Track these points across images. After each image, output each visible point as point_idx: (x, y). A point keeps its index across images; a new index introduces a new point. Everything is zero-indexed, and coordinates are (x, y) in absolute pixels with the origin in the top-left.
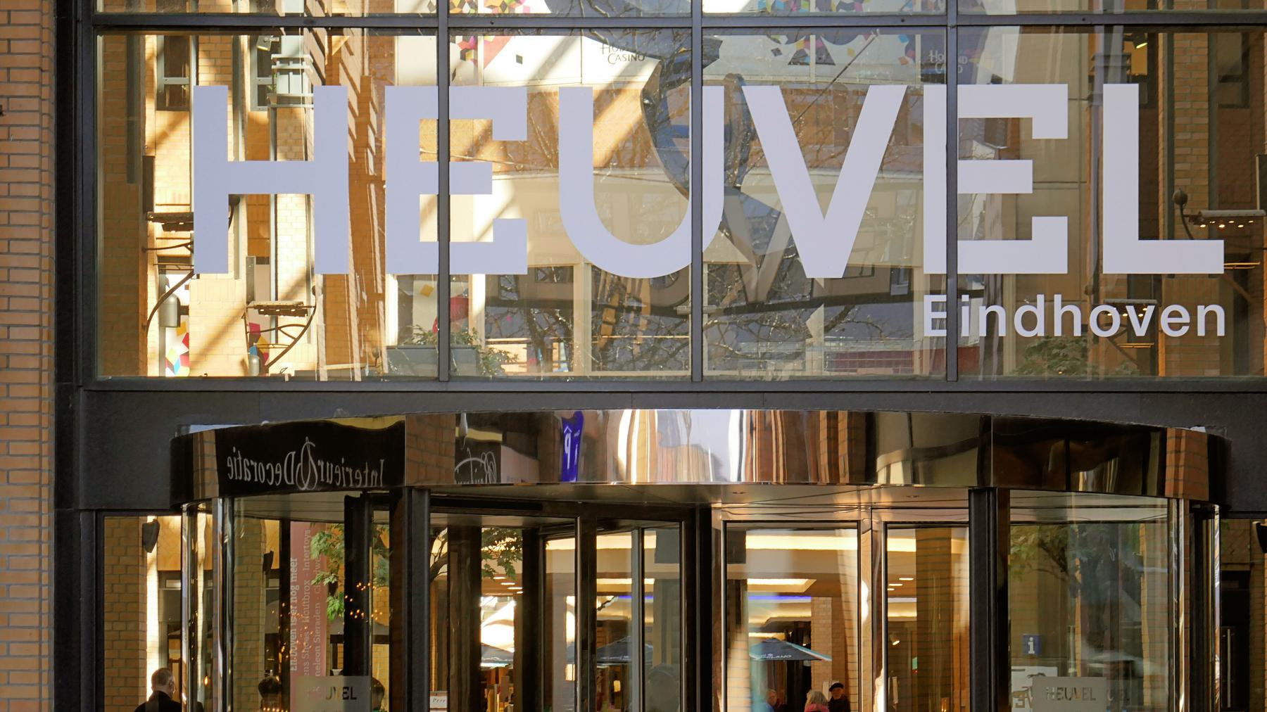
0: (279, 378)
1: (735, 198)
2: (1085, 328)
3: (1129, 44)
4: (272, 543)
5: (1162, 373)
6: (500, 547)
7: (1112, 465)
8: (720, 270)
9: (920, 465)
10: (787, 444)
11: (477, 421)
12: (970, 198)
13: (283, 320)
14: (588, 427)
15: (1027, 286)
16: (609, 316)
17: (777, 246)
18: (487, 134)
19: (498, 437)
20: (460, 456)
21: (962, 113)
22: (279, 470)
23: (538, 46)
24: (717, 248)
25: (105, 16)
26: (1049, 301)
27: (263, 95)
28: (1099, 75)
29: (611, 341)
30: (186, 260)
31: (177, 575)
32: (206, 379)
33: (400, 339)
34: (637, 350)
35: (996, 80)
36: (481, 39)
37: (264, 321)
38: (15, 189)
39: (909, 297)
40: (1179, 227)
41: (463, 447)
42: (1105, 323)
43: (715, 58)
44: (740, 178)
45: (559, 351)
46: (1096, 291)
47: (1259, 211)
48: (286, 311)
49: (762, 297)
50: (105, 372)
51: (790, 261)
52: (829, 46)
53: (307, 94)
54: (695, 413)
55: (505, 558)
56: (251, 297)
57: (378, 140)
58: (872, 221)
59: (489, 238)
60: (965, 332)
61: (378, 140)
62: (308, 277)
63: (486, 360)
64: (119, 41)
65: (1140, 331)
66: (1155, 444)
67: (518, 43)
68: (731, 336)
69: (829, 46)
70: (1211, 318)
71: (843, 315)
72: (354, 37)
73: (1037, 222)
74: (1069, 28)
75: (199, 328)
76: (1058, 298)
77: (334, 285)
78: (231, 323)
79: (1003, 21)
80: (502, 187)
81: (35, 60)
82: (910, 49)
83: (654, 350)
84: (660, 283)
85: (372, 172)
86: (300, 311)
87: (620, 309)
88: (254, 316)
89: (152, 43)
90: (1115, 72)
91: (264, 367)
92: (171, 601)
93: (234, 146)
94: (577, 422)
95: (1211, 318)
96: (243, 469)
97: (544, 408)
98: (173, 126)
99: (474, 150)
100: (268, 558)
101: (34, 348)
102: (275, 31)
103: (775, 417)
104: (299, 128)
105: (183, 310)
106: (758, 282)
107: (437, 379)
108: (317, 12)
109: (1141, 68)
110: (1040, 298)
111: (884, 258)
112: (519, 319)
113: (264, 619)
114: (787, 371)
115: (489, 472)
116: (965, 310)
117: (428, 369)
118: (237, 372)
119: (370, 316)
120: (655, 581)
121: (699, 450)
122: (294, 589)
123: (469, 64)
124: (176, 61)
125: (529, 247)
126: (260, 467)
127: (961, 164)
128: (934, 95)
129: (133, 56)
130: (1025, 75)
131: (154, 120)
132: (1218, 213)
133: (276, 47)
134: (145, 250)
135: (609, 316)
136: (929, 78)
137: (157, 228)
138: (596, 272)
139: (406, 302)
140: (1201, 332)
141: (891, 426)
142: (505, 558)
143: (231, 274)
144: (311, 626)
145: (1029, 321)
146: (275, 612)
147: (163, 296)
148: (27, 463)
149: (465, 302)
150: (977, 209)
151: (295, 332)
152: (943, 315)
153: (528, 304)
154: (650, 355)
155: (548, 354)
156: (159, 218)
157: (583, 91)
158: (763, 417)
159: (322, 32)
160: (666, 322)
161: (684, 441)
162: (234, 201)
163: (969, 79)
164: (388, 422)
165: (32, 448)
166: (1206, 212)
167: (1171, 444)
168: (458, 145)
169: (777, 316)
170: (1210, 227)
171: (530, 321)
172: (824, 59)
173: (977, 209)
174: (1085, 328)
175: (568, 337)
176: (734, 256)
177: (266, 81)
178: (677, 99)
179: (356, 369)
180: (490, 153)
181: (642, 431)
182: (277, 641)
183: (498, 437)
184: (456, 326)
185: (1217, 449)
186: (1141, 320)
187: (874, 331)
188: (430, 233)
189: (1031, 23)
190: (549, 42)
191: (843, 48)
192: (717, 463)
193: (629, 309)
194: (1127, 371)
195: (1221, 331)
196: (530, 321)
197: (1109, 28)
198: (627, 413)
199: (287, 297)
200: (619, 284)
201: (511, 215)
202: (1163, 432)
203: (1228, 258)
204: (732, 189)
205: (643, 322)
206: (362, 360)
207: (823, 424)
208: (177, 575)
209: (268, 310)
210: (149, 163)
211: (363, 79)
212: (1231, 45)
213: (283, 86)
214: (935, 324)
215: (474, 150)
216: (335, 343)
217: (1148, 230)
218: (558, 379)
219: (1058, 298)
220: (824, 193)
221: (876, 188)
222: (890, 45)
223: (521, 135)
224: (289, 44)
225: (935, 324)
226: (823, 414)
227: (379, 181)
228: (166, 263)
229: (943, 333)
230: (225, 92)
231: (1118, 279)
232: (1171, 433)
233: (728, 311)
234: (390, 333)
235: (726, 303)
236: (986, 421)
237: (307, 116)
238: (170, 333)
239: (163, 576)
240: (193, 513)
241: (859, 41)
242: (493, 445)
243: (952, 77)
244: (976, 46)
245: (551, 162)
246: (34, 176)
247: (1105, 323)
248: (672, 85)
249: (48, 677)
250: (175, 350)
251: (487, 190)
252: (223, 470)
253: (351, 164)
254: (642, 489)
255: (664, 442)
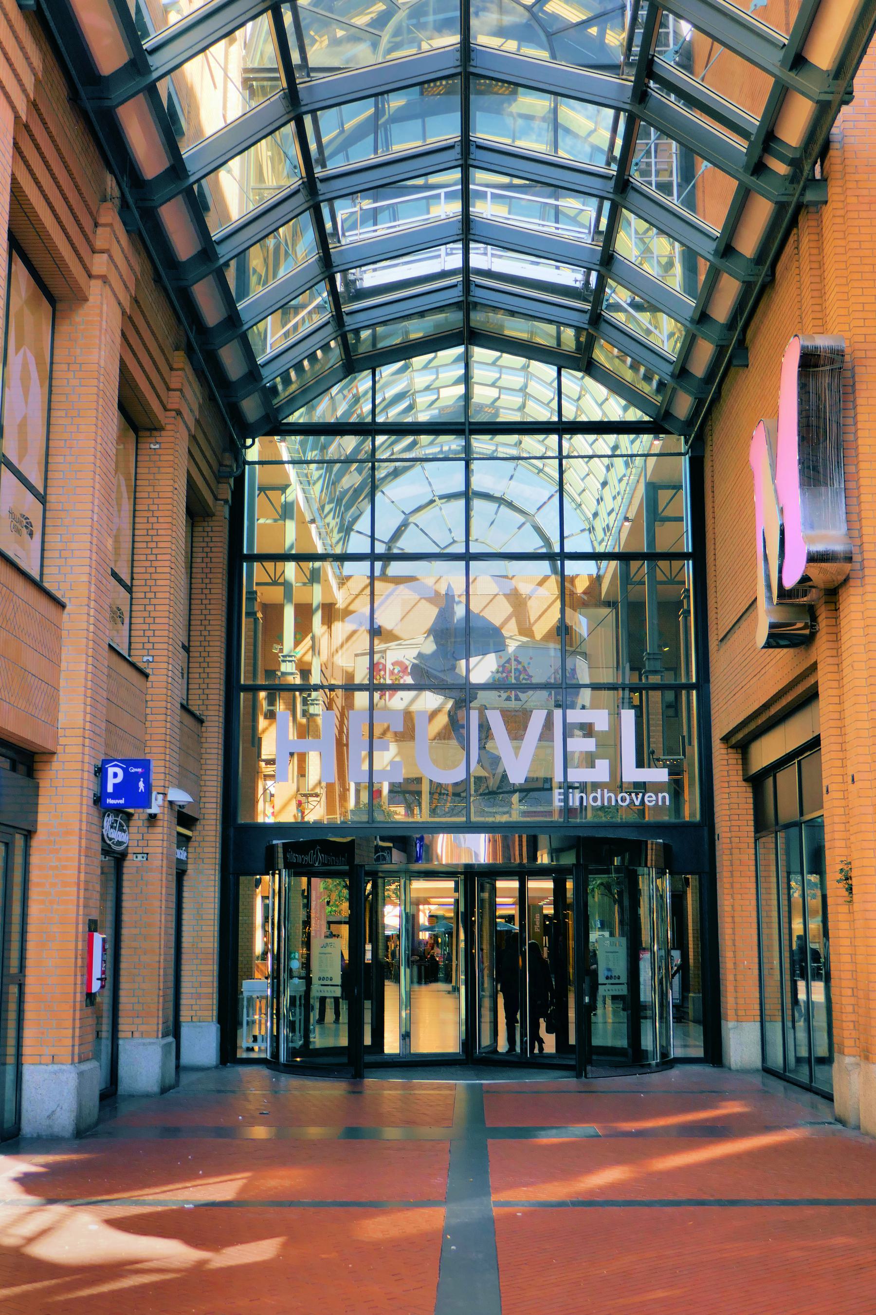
0: (308, 823)
1: (484, 751)
2: (617, 801)
3: (632, 694)
4: (304, 886)
5: (647, 819)
6: (393, 887)
7: (627, 856)
8: (479, 779)
9: (554, 855)
10: (503, 847)
11: (383, 839)
12: (573, 753)
13: (310, 799)
14: (426, 841)
15: (595, 786)
16: (436, 796)
17: (500, 770)
18: (388, 728)
19: (391, 845)
20: (376, 852)
21: (568, 721)
22: (307, 858)
23: (410, 694)
24: (476, 769)
25: (244, 685)
26: (602, 791)
27: (305, 713)
28: (621, 705)
29: (436, 806)
30: (273, 776)
31: (268, 898)
32: (279, 823)
33: (355, 806)
34: (447, 810)
35: (583, 707)
36: (387, 693)
37: (303, 799)
38: (208, 751)
39: (551, 789)
40: (652, 763)
41: (378, 849)
42: (623, 799)
43: (476, 698)
44: (485, 743)
45: (416, 810)
46: (621, 787)
47: (682, 757)
48: (311, 795)
49: (495, 789)
50: (242, 820)
51: (505, 777)
52: (520, 694)
53: (321, 713)
54: (467, 835)
55: (395, 891)
56: (298, 790)
57: (347, 730)
58: (536, 759)
59: (389, 768)
60: (571, 804)
61: (347, 730)
62: (320, 783)
63: (389, 814)
64: (250, 695)
65: (637, 803)
66: (643, 847)
67: (400, 694)
68: (483, 805)
69: (520, 694)
70: (664, 798)
71: (526, 795)
72: (340, 692)
73: (598, 762)
74: (609, 689)
75: (278, 802)
76: (606, 791)
77: (330, 787)
78: (290, 800)
79: (585, 686)
80: (393, 747)
81: (217, 702)
82: (550, 694)
83: (453, 810)
84: (456, 784)
85: (345, 742)
86: (317, 795)
87: (440, 794)
88: (300, 798)
89: (262, 695)
90: (626, 705)
91: (303, 817)
92: (266, 908)
93: (292, 734)
94: (421, 839)
95: (664, 798)
96: (294, 858)
97: (409, 834)
98: (270, 725)
99: (384, 733)
100: (303, 891)
101: (215, 811)
102: (309, 690)
103: (498, 837)
104: (317, 726)
105: (272, 795)
106: (493, 784)
107: (368, 822)
108: (325, 683)
109: (636, 702)
110: (599, 790)
111: (541, 774)
112: (401, 797)
113: (302, 915)
114: (504, 819)
115: (387, 858)
116: (571, 795)
117: (365, 818)
118: (292, 820)
119: (344, 797)
120: (368, 964)
121: (469, 850)
122: (313, 904)
123: (383, 701)
124: (271, 701)
125: (404, 771)
126: (300, 858)
127: (568, 739)
128: (558, 713)
129: (255, 700)
130: (593, 707)
131: (262, 723)
132: (666, 757)
133: (309, 695)
134: (258, 773)
135: (436, 796)
136: (558, 706)
137: (263, 764)
138: (431, 781)
139: (358, 792)
140: (660, 803)
141: (543, 840)
142: (395, 891)
143: (290, 781)
144: (320, 919)
145: (595, 799)
146: (305, 913)
147: (265, 790)
148: (210, 856)
149: (380, 792)
150: (577, 755)
151: (315, 803)
152: (562, 797)
153: (405, 792)
154: (452, 812)
155: (412, 811)
156: (264, 761)
157: (426, 712)
158: (494, 837)
159: (327, 691)
160: (457, 799)
161: (463, 846)
162: (292, 754)
163: (573, 706)
164: (349, 839)
165: (213, 850)
166: (662, 757)
167: (649, 846)
168: (377, 732)
169: (501, 796)
170: (664, 763)
171: (406, 799)
172: (517, 699)
173: (577, 755)
174: (617, 801)
175: (420, 805)
176: (484, 773)
177: (305, 708)
178: (461, 714)
179: (338, 819)
180: (389, 735)
181: (447, 842)
182: (307, 923)
183: (391, 845)
184: (375, 802)
185: (666, 848)
186: (637, 798)
187: (538, 802)
188: (365, 766)
189: (596, 687)
190: (413, 693)
191: (525, 694)
192: (477, 855)
193: (444, 794)
194: (632, 818)
195: (667, 803)
196: (406, 799)
197: (623, 689)
198: (441, 835)
199: (312, 790)
200: (440, 785)
201: (397, 759)
202: (646, 842)
203: (670, 774)
204: (482, 748)
205: (449, 798)
206: (340, 814)
207: (517, 839)
208: (268, 898)
209: (305, 795)
210: (260, 739)
211: (343, 708)
212: (670, 695)
213: (312, 710)
214: (560, 800)
215: (384, 733)
216: (330, 808)
217: (640, 764)
218: (418, 823)
219: (606, 791)
220: (517, 749)
221: (537, 747)
222: (544, 694)
223: (400, 728)
224: (314, 694)
225: (560, 800)
226: (517, 835)
227: (347, 745)
228: (266, 777)
229: (562, 804)
230: (289, 713)
231: (629, 783)
232: (649, 842)
233: (481, 795)
234: (351, 803)
235: (481, 791)
236: (579, 837)
237: (319, 720)
238: (267, 804)
239: (264, 898)
240: (273, 875)
241: (530, 692)
242: (389, 848)
243: (564, 706)
244: (577, 694)
245: (413, 738)
246: (216, 745)
247: (623, 799)
248: (460, 707)
249: (217, 939)
250: (269, 811)
251: (388, 750)
252: (285, 858)
253: (337, 739)
254: (447, 865)
255: (455, 847)
